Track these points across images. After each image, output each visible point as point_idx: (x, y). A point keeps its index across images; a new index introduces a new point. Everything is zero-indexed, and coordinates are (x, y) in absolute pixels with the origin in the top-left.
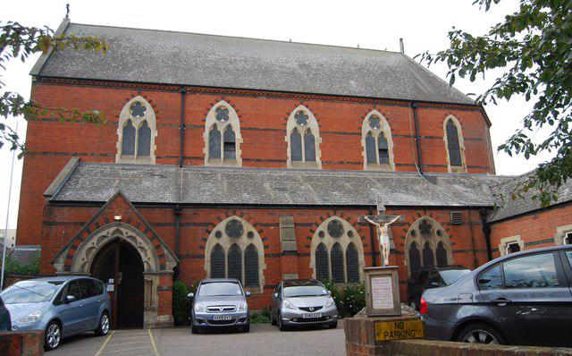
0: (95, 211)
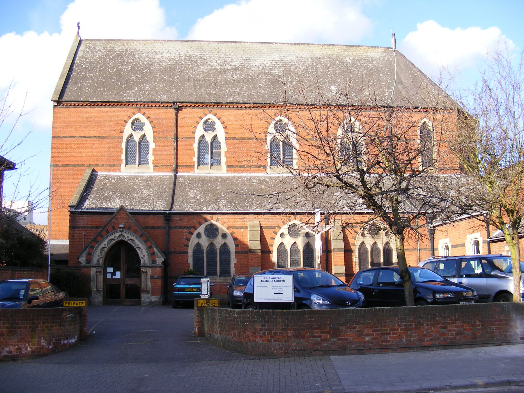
0: (106, 218)
